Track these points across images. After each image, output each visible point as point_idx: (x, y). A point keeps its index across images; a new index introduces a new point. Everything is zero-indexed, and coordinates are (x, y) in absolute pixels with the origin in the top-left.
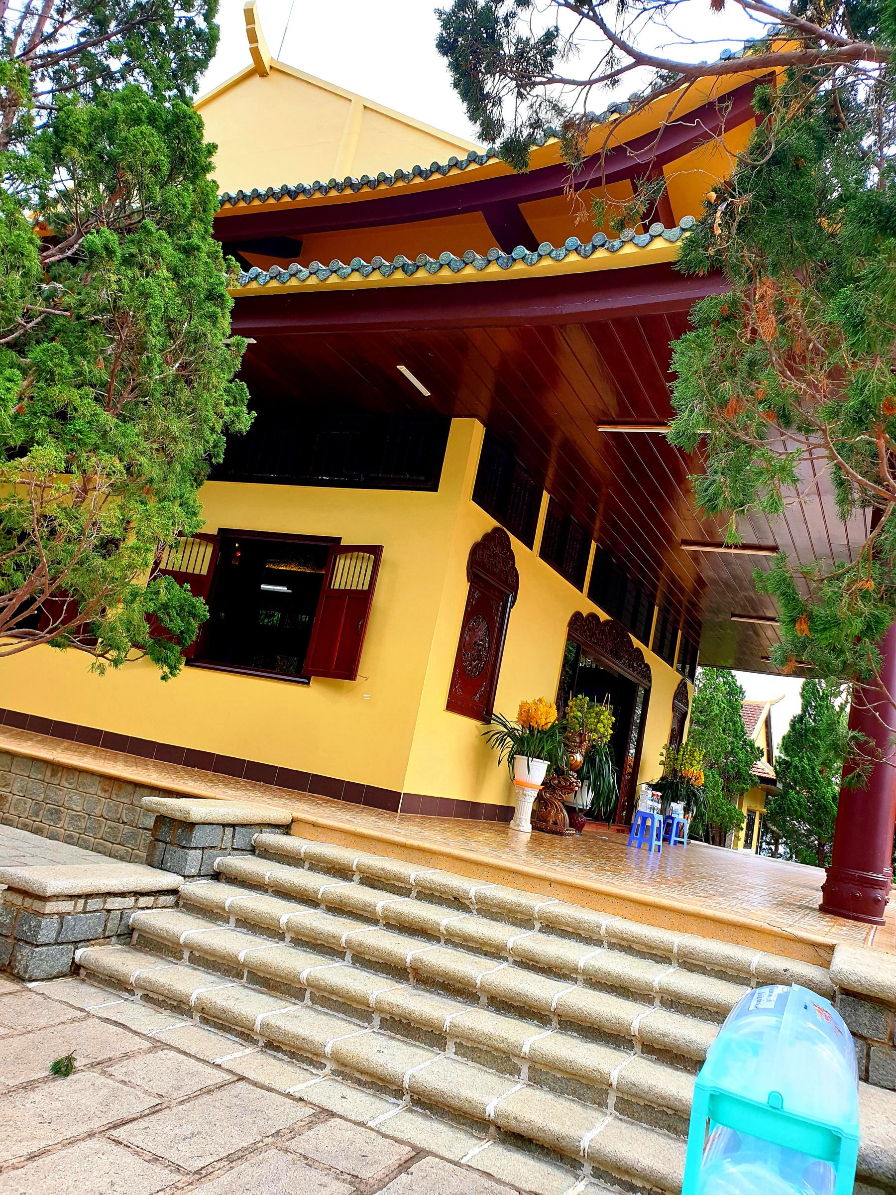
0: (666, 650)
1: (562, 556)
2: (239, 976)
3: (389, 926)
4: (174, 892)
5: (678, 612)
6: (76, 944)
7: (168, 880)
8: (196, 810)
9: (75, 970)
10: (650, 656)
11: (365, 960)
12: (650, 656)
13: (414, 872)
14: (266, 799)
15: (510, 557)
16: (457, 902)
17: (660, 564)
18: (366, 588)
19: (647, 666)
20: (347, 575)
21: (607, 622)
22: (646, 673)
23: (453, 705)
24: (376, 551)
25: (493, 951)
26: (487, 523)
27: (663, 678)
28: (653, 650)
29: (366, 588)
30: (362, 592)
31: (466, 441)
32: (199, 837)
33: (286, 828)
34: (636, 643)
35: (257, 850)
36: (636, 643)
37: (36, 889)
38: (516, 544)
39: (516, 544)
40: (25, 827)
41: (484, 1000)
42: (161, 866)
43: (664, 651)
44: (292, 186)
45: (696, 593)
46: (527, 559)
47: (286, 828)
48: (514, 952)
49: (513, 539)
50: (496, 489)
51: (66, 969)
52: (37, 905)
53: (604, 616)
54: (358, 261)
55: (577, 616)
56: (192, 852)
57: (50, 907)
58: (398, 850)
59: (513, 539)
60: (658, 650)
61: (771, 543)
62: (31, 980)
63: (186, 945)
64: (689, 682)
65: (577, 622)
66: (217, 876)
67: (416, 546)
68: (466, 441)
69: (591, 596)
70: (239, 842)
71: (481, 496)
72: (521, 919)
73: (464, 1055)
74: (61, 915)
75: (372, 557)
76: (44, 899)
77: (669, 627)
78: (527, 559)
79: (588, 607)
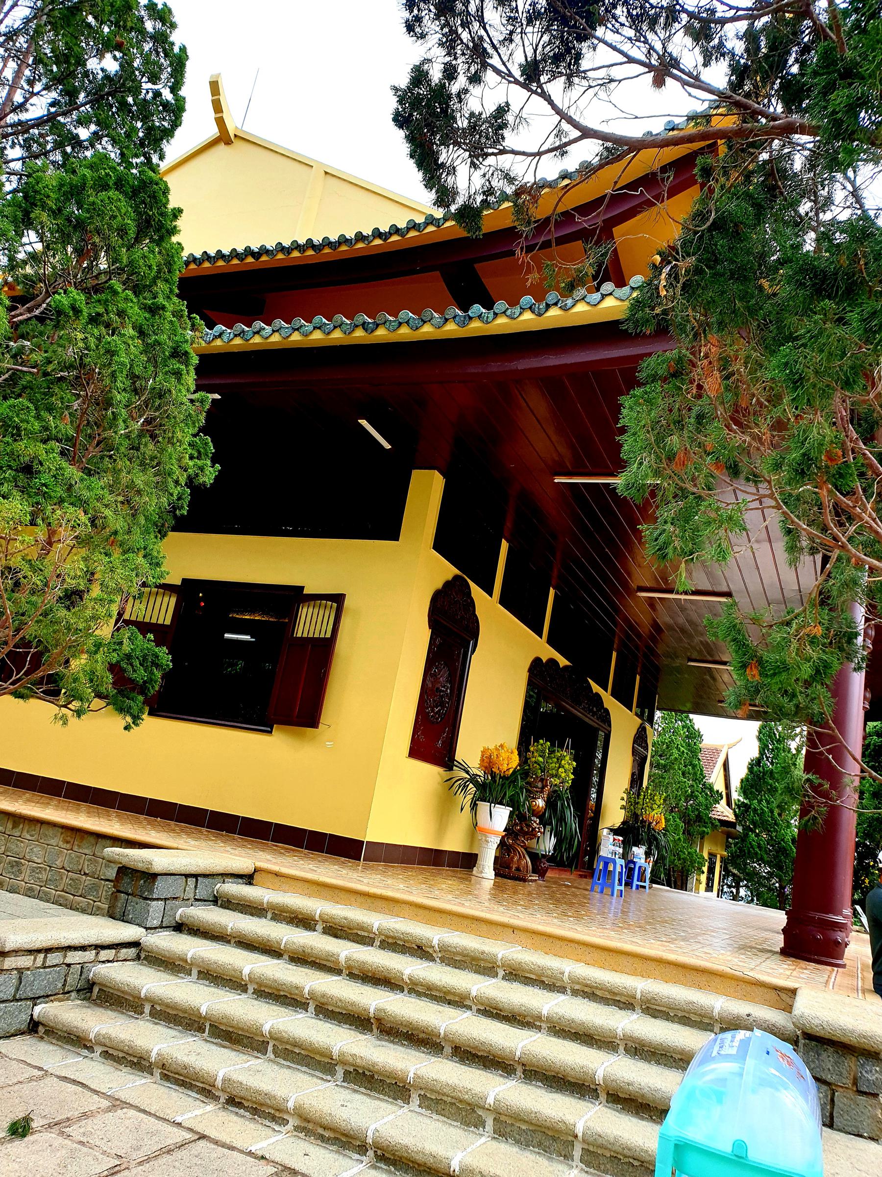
1: (522, 604)
2: (201, 1029)
3: (352, 976)
4: (136, 944)
6: (35, 1000)
8: (158, 860)
9: (34, 1027)
10: (610, 702)
12: (610, 702)
15: (471, 604)
16: (421, 951)
18: (328, 635)
19: (607, 711)
21: (566, 667)
24: (338, 599)
26: (448, 570)
29: (328, 635)
32: (161, 888)
33: (248, 878)
34: (596, 688)
35: (216, 900)
36: (596, 688)
38: (476, 591)
39: (476, 591)
41: (448, 1050)
42: (123, 918)
43: (623, 696)
46: (487, 606)
47: (248, 878)
48: (478, 1000)
49: (472, 584)
51: (24, 1027)
53: (563, 662)
54: (320, 319)
55: (537, 661)
58: (360, 899)
61: (724, 589)
63: (147, 999)
65: (538, 669)
66: (179, 928)
67: (378, 597)
69: (549, 642)
70: (201, 893)
71: (440, 545)
73: (428, 1108)
75: (335, 605)
78: (487, 606)
79: (548, 653)
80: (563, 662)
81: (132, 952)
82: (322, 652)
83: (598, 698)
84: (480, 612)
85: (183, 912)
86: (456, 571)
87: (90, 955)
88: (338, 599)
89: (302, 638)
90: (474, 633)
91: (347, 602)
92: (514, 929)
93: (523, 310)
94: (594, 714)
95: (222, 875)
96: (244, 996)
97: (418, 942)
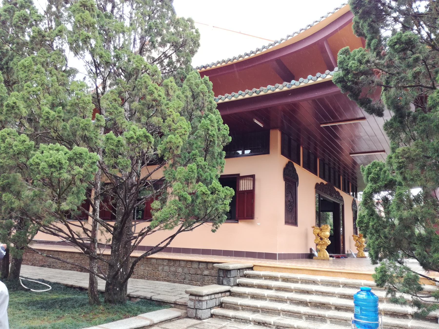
0: (347, 190)
1: (310, 166)
2: (258, 312)
3: (296, 292)
4: (229, 291)
5: (349, 176)
6: (211, 308)
7: (227, 288)
8: (231, 266)
9: (212, 316)
10: (342, 193)
11: (293, 302)
12: (342, 193)
13: (299, 276)
14: (249, 261)
15: (295, 170)
16: (314, 282)
17: (339, 159)
18: (252, 189)
19: (341, 197)
20: (244, 186)
21: (326, 184)
22: (341, 199)
23: (287, 222)
24: (253, 177)
25: (332, 295)
26: (286, 160)
27: (347, 199)
28: (343, 191)
29: (252, 189)
30: (251, 190)
31: (276, 138)
32: (233, 273)
33: (251, 268)
34: (337, 189)
35: (245, 276)
36: (337, 189)
37: (201, 294)
38: (296, 166)
39: (296, 166)
40: (165, 280)
41: (333, 308)
42: (222, 284)
43: (346, 190)
44: (204, 65)
45: (354, 167)
46: (300, 170)
47: (251, 268)
48: (338, 294)
49: (294, 163)
50: (288, 151)
51: (210, 316)
52: (200, 298)
53: (325, 183)
54: (240, 92)
55: (317, 185)
56: (231, 278)
57: (204, 298)
58: (289, 270)
59: (294, 163)
60: (344, 190)
61: (382, 149)
62: (203, 319)
63: (240, 305)
64: (355, 199)
65: (318, 187)
66: (238, 285)
67: (266, 173)
68: (276, 138)
69: (320, 177)
70: (241, 274)
71: (283, 153)
72: (337, 285)
73: (333, 323)
74: (207, 300)
75: (252, 178)
76: (202, 296)
77: (346, 181)
78: (300, 170)
79: (320, 180)
80: (325, 183)
81: (228, 294)
82: (251, 194)
83: (338, 193)
84: (298, 172)
85: (239, 280)
86: (289, 160)
87: (220, 295)
88: (253, 177)
89: (242, 191)
90: (297, 179)
91: (256, 177)
92: (341, 273)
93: (309, 80)
94: (338, 199)
95: (245, 268)
96: (266, 302)
97: (313, 280)
